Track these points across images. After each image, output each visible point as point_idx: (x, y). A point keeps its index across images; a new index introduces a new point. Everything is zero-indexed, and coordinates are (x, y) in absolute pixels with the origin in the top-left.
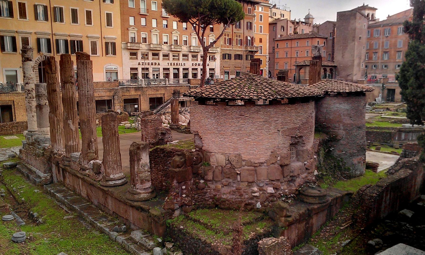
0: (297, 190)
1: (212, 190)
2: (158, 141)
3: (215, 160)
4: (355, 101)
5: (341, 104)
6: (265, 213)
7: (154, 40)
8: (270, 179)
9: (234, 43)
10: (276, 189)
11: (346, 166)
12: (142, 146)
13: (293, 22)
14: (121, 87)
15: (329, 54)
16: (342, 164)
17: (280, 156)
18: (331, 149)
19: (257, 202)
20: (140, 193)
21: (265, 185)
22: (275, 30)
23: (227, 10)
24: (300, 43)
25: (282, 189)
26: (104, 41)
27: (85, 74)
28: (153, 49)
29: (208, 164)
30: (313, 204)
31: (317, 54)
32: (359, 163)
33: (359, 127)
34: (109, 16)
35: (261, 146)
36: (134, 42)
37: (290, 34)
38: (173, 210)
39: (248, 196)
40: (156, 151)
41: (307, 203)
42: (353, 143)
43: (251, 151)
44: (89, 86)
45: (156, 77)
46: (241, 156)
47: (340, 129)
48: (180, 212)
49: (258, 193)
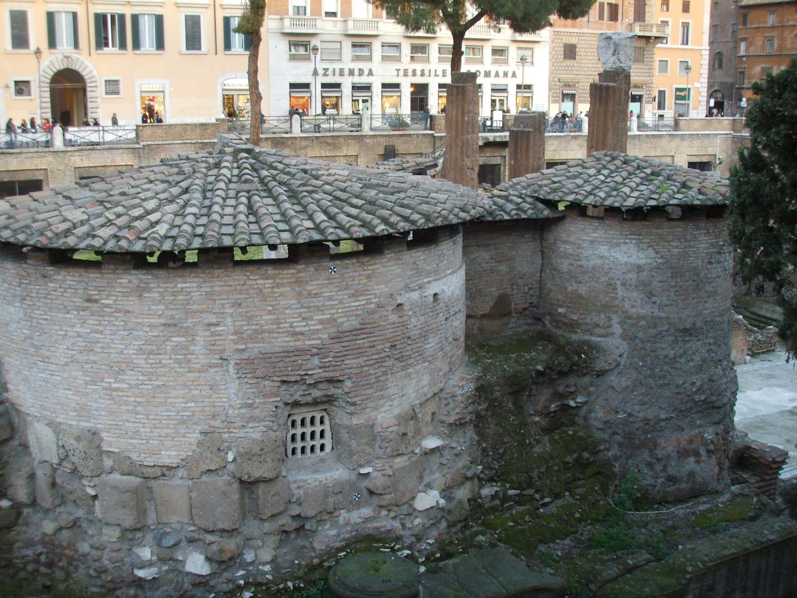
5: (618, 245)
8: (199, 522)
17: (234, 449)
33: (685, 331)
42: (661, 386)
43: (131, 425)
46: (101, 439)
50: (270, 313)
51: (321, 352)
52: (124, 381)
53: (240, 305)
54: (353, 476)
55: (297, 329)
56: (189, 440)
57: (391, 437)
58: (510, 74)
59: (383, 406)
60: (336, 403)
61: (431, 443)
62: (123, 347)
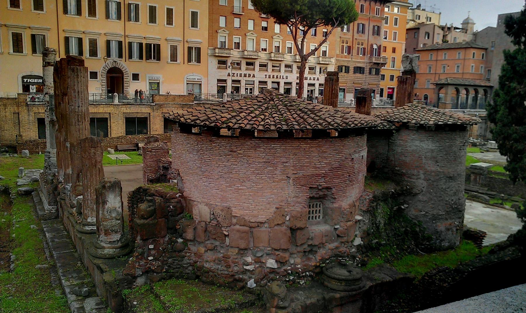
0: (316, 267)
1: (193, 254)
2: (159, 177)
3: (198, 212)
4: (445, 138)
5: (424, 141)
6: (259, 297)
7: (250, 46)
8: (273, 246)
9: (355, 51)
10: (281, 262)
11: (426, 232)
12: (108, 184)
13: (443, 28)
14: (196, 102)
15: (489, 70)
16: (420, 229)
17: (289, 215)
18: (403, 207)
19: (250, 278)
20: (104, 248)
21: (265, 255)
22: (416, 36)
23: (332, 8)
24: (448, 55)
25: (292, 263)
26: (186, 46)
27: (76, 84)
28: (247, 57)
29: (190, 216)
30: (334, 290)
31: (408, 67)
32: (448, 230)
33: (450, 178)
34: (194, 15)
35: (260, 197)
36: (223, 47)
37: (436, 43)
38: (135, 278)
39: (238, 269)
40: (139, 192)
41: (327, 287)
42: (439, 201)
43: (246, 204)
44: (80, 100)
45: (249, 92)
46: (232, 211)
47: (420, 178)
48: (146, 279)
49: (253, 266)
50: (307, 158)
51: (325, 176)
52: (244, 186)
53: (296, 154)
54: (333, 229)
55: (317, 166)
56: (271, 211)
57: (347, 213)
58: (316, 79)
59: (344, 200)
60: (326, 198)
61: (359, 218)
62: (246, 171)
